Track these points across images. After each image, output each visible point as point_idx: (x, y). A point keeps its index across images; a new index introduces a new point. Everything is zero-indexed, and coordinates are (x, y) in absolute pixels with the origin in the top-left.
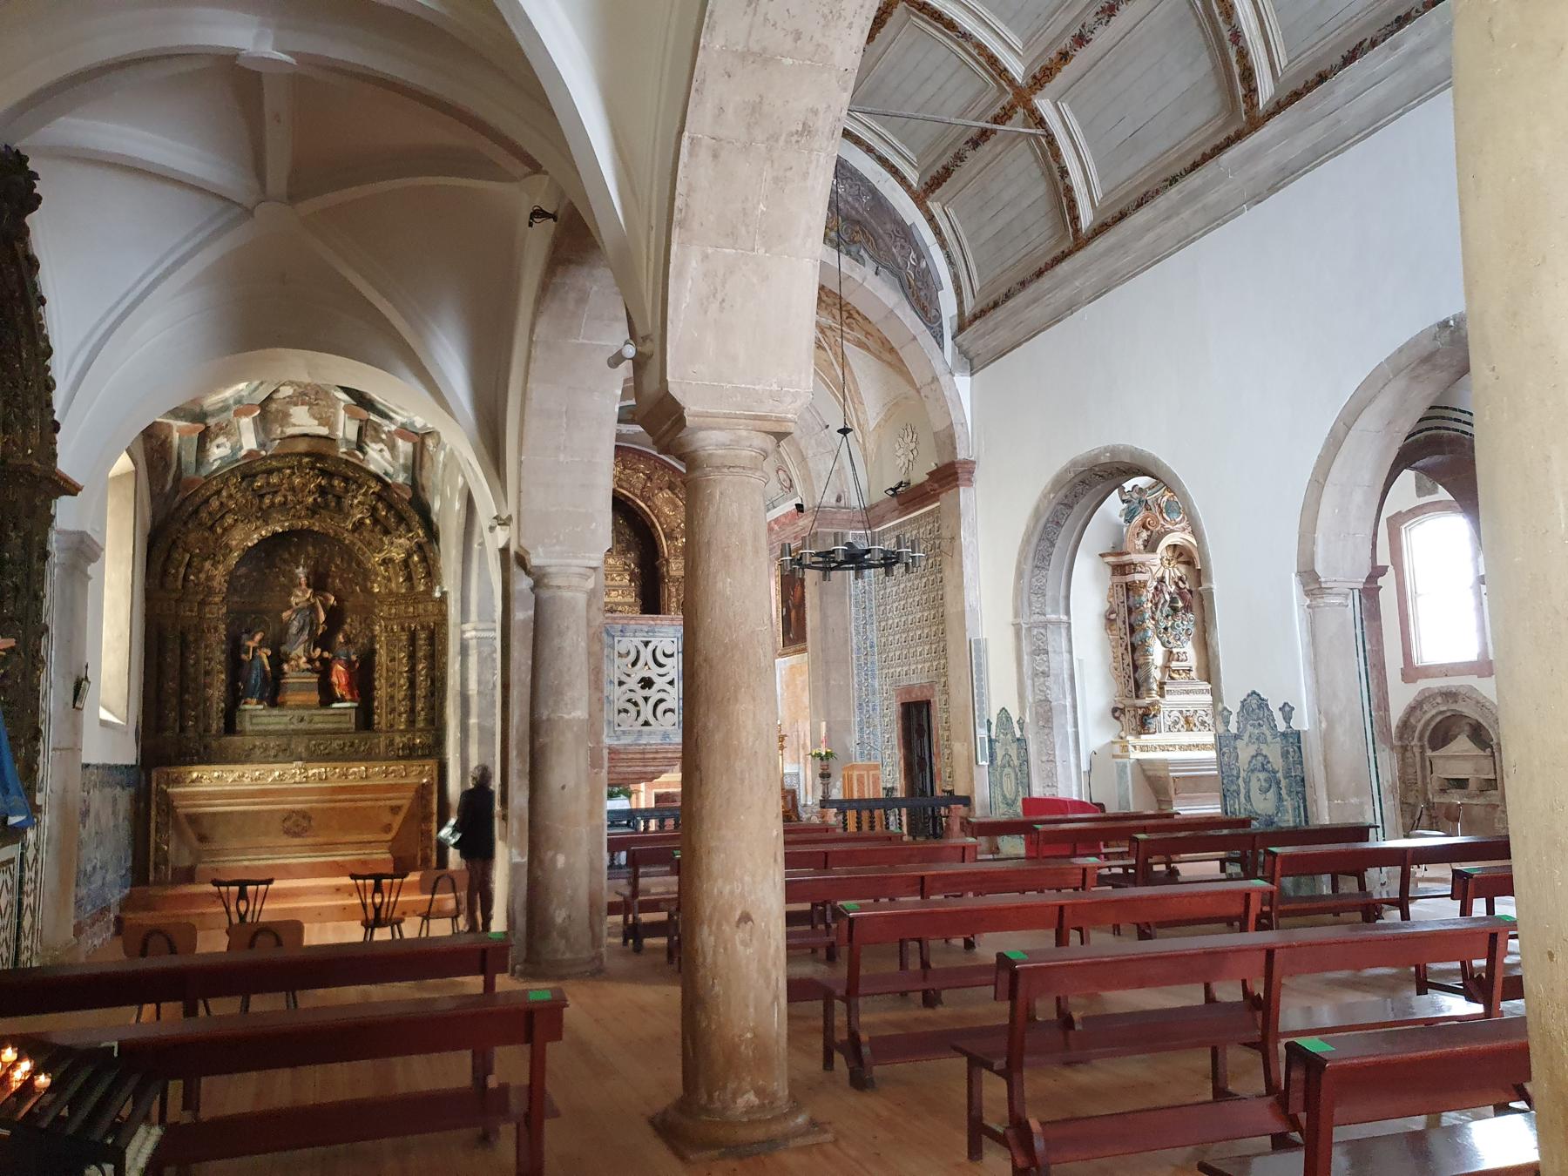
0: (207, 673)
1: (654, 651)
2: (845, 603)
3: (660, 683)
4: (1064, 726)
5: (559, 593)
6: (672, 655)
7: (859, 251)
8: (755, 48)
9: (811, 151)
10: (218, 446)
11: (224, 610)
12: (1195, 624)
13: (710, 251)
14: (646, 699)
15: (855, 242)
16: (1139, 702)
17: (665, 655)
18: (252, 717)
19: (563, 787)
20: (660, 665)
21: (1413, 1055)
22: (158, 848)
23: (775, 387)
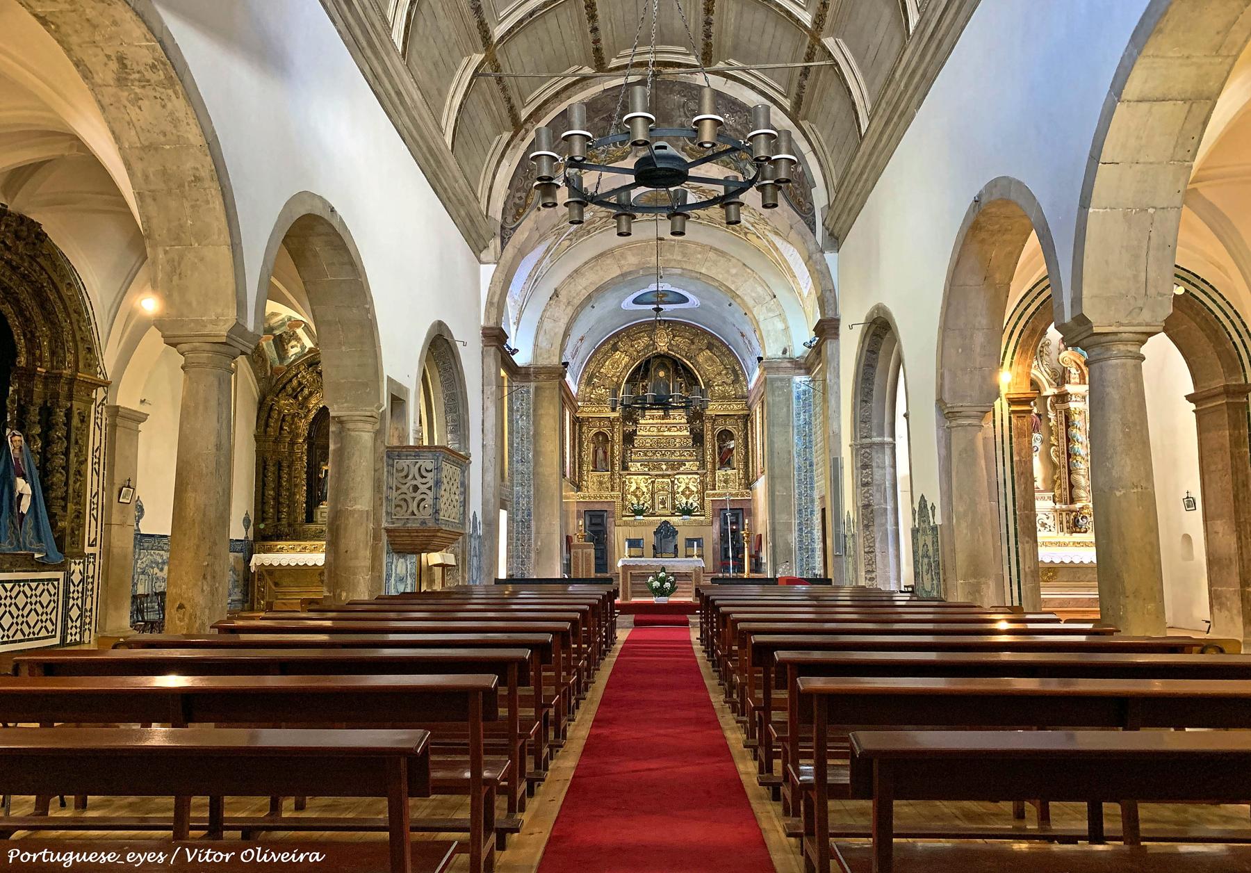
0: (296, 485)
1: (419, 469)
2: (788, 432)
3: (423, 488)
4: (884, 525)
5: (352, 433)
6: (431, 471)
7: (745, 166)
8: (146, 143)
9: (205, 189)
10: (292, 347)
11: (306, 447)
12: (1042, 442)
13: (168, 248)
14: (414, 498)
15: (742, 160)
16: (1072, 507)
17: (427, 471)
18: (321, 513)
19: (346, 552)
20: (423, 477)
21: (312, 685)
22: (259, 590)
23: (214, 317)
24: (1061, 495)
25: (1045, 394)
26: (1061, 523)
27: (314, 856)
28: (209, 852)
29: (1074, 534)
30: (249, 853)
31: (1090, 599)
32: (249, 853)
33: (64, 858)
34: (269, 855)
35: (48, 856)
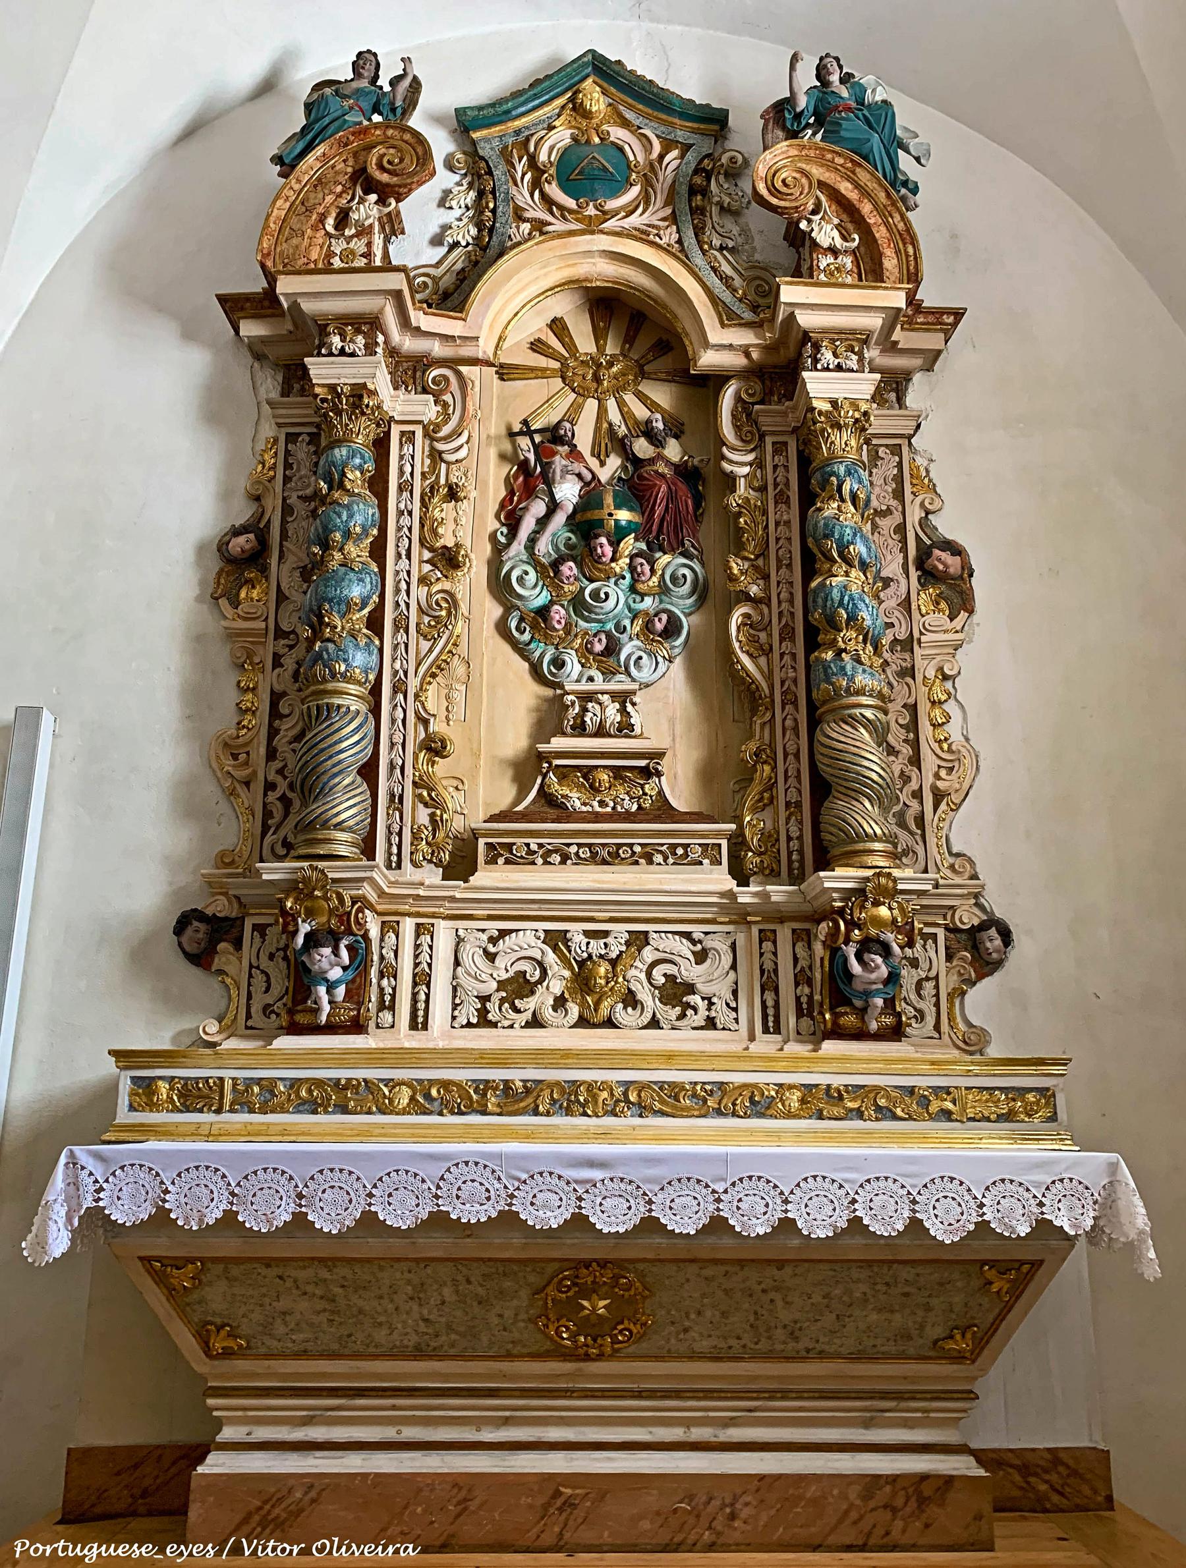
24: (770, 838)
25: (708, 359)
26: (769, 984)
27: (407, 1548)
28: (271, 1543)
29: (830, 1047)
30: (324, 1546)
31: (874, 1481)
32: (324, 1546)
33: (86, 1551)
34: (349, 1548)
35: (65, 1549)
